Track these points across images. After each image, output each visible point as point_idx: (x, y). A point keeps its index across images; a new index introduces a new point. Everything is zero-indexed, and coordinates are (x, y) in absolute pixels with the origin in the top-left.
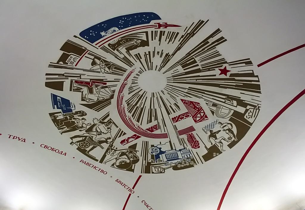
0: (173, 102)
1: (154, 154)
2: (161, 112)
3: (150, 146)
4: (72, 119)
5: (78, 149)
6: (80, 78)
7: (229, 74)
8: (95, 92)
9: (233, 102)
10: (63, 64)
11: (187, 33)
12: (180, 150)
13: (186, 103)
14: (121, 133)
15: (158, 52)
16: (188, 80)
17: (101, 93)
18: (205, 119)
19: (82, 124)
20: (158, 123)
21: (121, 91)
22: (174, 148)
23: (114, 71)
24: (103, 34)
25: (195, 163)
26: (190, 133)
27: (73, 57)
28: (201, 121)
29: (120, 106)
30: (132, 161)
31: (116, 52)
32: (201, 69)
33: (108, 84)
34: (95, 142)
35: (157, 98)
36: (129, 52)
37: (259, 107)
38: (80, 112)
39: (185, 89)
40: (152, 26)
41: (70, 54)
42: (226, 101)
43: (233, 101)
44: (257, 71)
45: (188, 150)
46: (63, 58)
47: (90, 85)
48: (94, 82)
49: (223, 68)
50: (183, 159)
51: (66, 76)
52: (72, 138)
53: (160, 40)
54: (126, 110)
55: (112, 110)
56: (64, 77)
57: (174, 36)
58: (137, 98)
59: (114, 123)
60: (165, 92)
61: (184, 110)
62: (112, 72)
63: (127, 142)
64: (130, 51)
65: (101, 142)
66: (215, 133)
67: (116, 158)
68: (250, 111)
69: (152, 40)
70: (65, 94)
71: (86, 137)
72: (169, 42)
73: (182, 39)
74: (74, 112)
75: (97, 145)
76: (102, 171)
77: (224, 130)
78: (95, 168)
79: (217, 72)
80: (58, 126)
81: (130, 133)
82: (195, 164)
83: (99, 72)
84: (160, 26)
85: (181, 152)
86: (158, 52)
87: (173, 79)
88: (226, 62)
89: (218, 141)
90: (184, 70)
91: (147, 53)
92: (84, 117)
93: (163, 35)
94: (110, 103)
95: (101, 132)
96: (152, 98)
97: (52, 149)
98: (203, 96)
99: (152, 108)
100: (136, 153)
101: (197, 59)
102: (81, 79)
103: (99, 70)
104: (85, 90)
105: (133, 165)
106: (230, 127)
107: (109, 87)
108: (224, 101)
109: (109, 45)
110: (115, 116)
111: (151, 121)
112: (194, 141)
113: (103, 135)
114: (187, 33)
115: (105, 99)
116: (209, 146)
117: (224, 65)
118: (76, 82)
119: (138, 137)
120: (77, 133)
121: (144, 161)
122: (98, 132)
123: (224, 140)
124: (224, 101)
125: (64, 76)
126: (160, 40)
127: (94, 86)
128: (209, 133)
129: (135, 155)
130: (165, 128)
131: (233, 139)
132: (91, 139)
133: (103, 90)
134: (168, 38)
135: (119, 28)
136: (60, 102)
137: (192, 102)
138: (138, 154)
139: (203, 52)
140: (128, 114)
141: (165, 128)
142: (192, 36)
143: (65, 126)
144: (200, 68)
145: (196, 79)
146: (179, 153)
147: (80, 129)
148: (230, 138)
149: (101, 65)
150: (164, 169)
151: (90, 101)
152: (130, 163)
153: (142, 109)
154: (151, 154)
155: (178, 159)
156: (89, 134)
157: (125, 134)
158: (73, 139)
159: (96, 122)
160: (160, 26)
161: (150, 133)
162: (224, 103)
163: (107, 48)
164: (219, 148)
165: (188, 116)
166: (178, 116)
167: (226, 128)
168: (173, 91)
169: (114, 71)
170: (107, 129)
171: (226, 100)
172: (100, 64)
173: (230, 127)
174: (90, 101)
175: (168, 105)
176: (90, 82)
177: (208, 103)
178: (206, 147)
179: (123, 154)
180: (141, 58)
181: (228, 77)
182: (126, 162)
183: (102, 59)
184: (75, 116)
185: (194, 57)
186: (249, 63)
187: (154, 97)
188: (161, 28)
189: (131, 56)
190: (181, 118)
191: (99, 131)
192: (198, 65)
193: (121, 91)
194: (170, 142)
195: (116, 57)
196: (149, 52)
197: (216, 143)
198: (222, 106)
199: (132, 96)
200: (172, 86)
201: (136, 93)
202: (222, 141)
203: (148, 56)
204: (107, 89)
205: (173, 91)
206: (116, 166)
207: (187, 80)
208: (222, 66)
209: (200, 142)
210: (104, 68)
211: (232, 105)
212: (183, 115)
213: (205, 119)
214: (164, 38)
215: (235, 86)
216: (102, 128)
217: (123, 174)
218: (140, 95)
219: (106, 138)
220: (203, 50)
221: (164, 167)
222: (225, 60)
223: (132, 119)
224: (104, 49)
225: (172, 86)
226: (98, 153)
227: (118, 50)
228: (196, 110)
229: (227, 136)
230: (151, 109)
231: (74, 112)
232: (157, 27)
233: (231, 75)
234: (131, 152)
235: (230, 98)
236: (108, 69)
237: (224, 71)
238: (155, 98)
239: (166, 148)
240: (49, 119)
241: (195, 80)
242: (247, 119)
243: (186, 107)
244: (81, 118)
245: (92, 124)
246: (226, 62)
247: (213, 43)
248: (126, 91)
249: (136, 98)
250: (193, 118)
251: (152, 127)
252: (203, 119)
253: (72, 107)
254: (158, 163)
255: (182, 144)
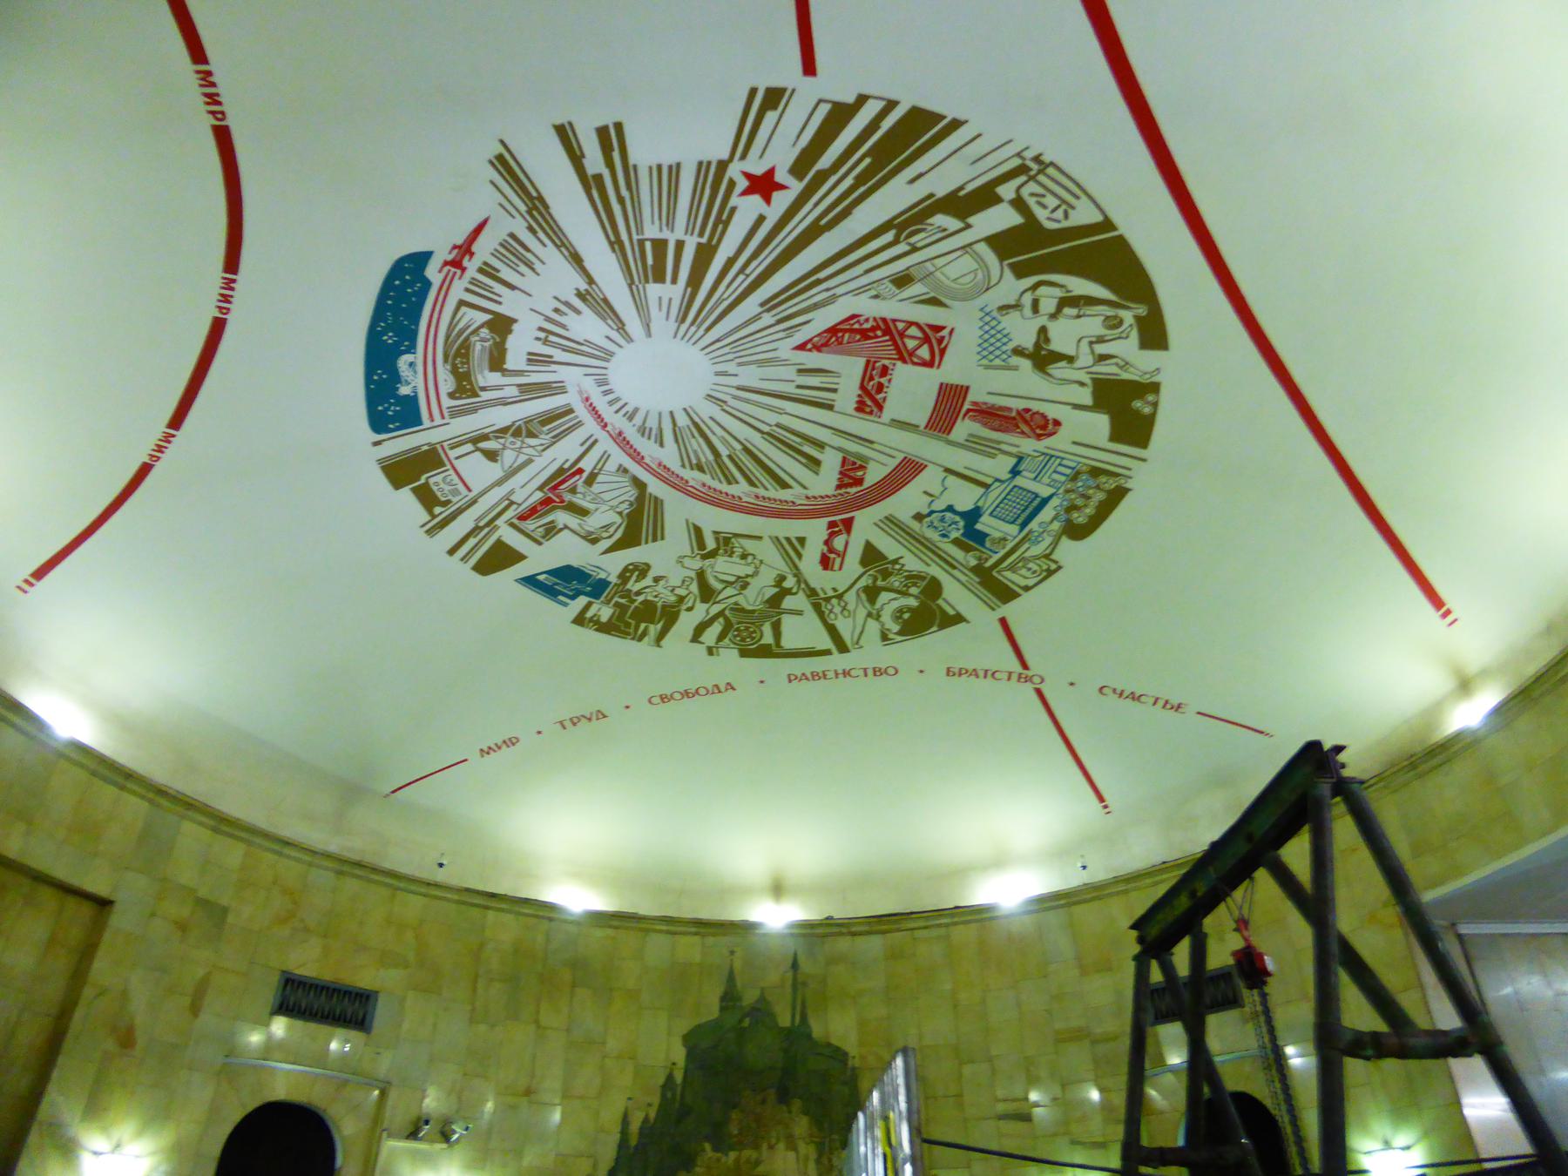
0: (782, 372)
1: (955, 535)
2: (800, 418)
3: (915, 525)
4: (635, 598)
5: (744, 653)
6: (515, 506)
7: (781, 176)
8: (591, 506)
9: (932, 225)
10: (443, 509)
11: (525, 214)
12: (1015, 472)
13: (826, 344)
14: (793, 548)
15: (556, 310)
16: (726, 293)
17: (606, 496)
18: (943, 338)
19: (672, 591)
20: (840, 449)
21: (637, 457)
22: (989, 481)
23: (550, 431)
24: (404, 390)
25: (1117, 475)
26: (966, 407)
27: (437, 481)
28: (943, 352)
29: (690, 489)
30: (920, 593)
31: (485, 396)
32: (704, 240)
33: (587, 465)
34: (759, 610)
35: (735, 397)
36: (506, 370)
37: (1037, 159)
38: (626, 569)
39: (757, 318)
40: (446, 286)
41: (423, 480)
42: (913, 240)
43: (930, 221)
44: (835, 83)
45: (1036, 454)
46: (427, 498)
47: (558, 500)
48: (555, 487)
49: (742, 184)
50: (1061, 491)
51: (487, 525)
52: (696, 638)
53: (512, 287)
54: (715, 484)
55: (679, 511)
56: (486, 530)
57: (518, 251)
58: (694, 437)
59: (736, 535)
60: (731, 368)
61: (848, 369)
62: (553, 437)
63: (839, 555)
64: (505, 366)
65: (775, 602)
66: (1037, 345)
67: (869, 615)
68: (1032, 195)
69: (500, 303)
70: (541, 558)
71: (721, 613)
72: (533, 269)
73: (541, 235)
74: (613, 579)
75: (775, 614)
76: (878, 672)
77: (1053, 316)
78: (846, 673)
79: (749, 207)
80: (628, 634)
81: (815, 531)
82: (1123, 481)
83: (529, 462)
84: (457, 264)
85: (1024, 473)
86: (556, 310)
87: (692, 324)
88: (723, 166)
89: (1085, 359)
90: (674, 281)
91: (542, 335)
92: (651, 574)
93: (498, 271)
94: (658, 503)
95: (739, 577)
96: (725, 407)
97: (686, 694)
98: (827, 290)
99: (766, 429)
100: (903, 565)
101: (652, 231)
102: (520, 505)
103: (522, 458)
104: (561, 517)
105: (940, 602)
106: (1058, 293)
107: (600, 469)
108: (908, 248)
109: (451, 395)
110: (715, 520)
111: (817, 463)
112: (1014, 419)
113: (755, 584)
114: (525, 214)
115: (632, 499)
116: (1085, 397)
117: (734, 171)
118: (522, 518)
119: (848, 524)
120: (687, 622)
121: (955, 572)
122: (732, 583)
123: (1101, 340)
124: (902, 247)
125: (482, 528)
126: (512, 287)
127: (568, 497)
128: (1026, 364)
129: (906, 574)
130: (875, 446)
131: (1128, 316)
132: (738, 609)
133: (596, 488)
134: (518, 266)
135: (408, 351)
136: (557, 584)
137: (833, 330)
138: (912, 564)
139: (669, 193)
140: (733, 490)
141: (875, 446)
142: (546, 207)
143: (643, 626)
144: (699, 244)
145: (742, 270)
146: (1019, 481)
147: (684, 607)
148: (1114, 323)
149: (507, 445)
150: (1047, 557)
151: (612, 530)
152: (922, 604)
153: (746, 450)
154: (946, 540)
155: (1045, 501)
156: (718, 602)
157: (802, 540)
158: (701, 639)
159: (697, 564)
160: (457, 264)
161: (859, 489)
162: (914, 249)
163: (462, 405)
164: (1125, 376)
165: (885, 371)
166: (860, 392)
167: (1048, 305)
168: (765, 340)
169: (550, 431)
170: (743, 562)
171: (907, 237)
172: (504, 445)
173: (1058, 293)
174: (612, 530)
175: (790, 389)
176: (546, 494)
177: (873, 293)
178: (1076, 407)
179: (872, 593)
180: (551, 357)
181: (796, 187)
182: (910, 609)
183: (492, 432)
184: (628, 586)
185: (635, 237)
186: (774, 97)
187: (725, 402)
188: (466, 262)
189: (526, 374)
190: (880, 388)
191: (732, 579)
192: (680, 245)
193: (637, 457)
194: (948, 470)
195: (504, 402)
196: (541, 329)
197: (1090, 370)
198: (928, 264)
199: (675, 446)
200: (718, 340)
201: (674, 431)
202: (1101, 349)
203: (552, 338)
204: (600, 478)
205: (765, 340)
206: (896, 633)
207: (725, 296)
208: (732, 184)
209: (1036, 406)
210: (524, 445)
211: (946, 233)
212: (867, 376)
213: (943, 338)
214: (506, 273)
215: (860, 181)
216: (725, 567)
217: (935, 645)
218: (688, 426)
219: (774, 584)
220: (621, 200)
221: (1036, 550)
222: (709, 163)
223: (761, 492)
224: (456, 413)
225: (718, 340)
226: (801, 629)
227: (484, 389)
228: (877, 337)
229: (1093, 324)
230: (768, 434)
231: (613, 579)
232: (455, 273)
233: (798, 169)
234: (886, 574)
235: (908, 223)
236: (534, 440)
237: (764, 185)
238: (732, 402)
239: (965, 497)
240: (589, 635)
241: (741, 277)
242: (1065, 224)
243: (835, 352)
244: (648, 581)
245: (693, 574)
246: (723, 166)
247: (610, 164)
248: (647, 448)
249: (693, 441)
250: (904, 361)
251: (841, 473)
252: (940, 341)
253: (594, 574)
254: (1002, 553)
255: (997, 452)
